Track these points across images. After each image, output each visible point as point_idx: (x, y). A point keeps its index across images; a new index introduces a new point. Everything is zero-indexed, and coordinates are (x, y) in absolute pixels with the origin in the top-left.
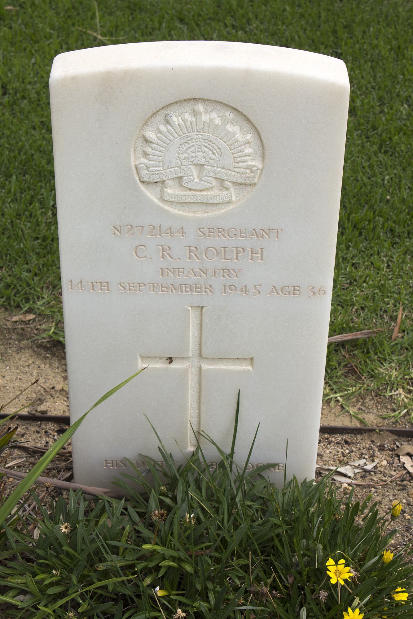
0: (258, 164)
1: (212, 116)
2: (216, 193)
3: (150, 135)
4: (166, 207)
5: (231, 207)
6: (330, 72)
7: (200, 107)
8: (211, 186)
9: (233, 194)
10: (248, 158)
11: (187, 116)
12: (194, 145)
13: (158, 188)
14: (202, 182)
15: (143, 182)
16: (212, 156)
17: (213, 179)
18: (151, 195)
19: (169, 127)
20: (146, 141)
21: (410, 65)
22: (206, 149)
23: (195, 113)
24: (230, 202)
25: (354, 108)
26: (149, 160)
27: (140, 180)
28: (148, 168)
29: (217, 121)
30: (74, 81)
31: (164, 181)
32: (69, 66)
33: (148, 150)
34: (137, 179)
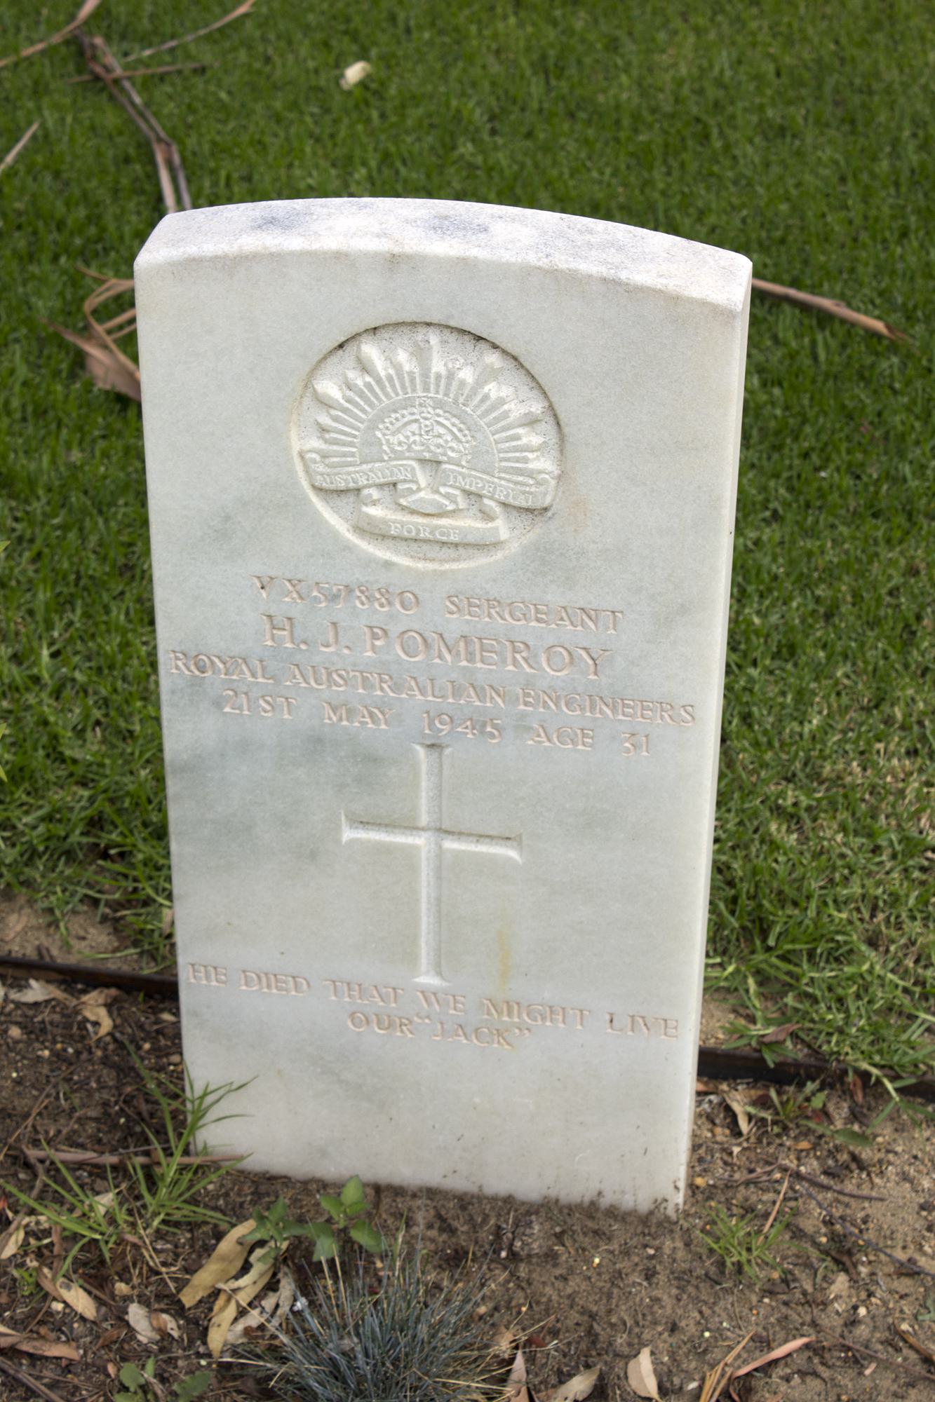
0: (544, 464)
1: (443, 358)
2: (469, 524)
3: (329, 387)
4: (381, 553)
5: (499, 555)
6: (720, 278)
7: (434, 338)
8: (450, 508)
9: (501, 527)
10: (530, 456)
11: (402, 356)
12: (416, 421)
13: (347, 502)
14: (437, 497)
15: (318, 490)
16: (454, 445)
17: (457, 492)
18: (333, 518)
19: (368, 379)
20: (325, 403)
21: (918, 211)
22: (442, 431)
23: (421, 354)
24: (497, 545)
25: (76, 590)
26: (326, 441)
27: (313, 486)
28: (324, 456)
29: (467, 375)
30: (187, 267)
31: (359, 490)
32: (185, 243)
33: (325, 420)
34: (305, 484)
